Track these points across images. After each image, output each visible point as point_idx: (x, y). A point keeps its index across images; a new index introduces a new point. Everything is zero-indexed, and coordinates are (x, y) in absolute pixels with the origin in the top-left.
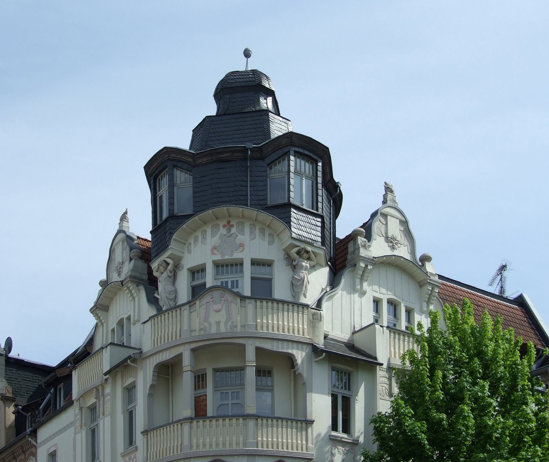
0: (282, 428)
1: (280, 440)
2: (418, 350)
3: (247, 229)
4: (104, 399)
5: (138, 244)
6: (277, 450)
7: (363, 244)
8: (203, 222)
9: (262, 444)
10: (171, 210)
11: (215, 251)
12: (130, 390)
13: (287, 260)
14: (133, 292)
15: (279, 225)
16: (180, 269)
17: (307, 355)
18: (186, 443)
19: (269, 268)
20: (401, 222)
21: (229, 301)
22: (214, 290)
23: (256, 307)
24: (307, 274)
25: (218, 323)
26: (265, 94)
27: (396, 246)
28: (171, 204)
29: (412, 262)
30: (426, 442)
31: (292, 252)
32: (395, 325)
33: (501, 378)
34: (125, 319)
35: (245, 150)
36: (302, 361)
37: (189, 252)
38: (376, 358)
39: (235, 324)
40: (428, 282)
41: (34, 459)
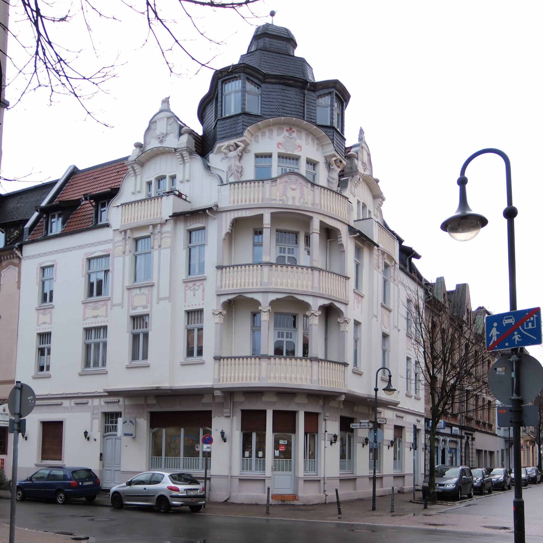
11: (280, 146)
16: (246, 151)
19: (270, 159)
37: (257, 142)
39: (306, 201)
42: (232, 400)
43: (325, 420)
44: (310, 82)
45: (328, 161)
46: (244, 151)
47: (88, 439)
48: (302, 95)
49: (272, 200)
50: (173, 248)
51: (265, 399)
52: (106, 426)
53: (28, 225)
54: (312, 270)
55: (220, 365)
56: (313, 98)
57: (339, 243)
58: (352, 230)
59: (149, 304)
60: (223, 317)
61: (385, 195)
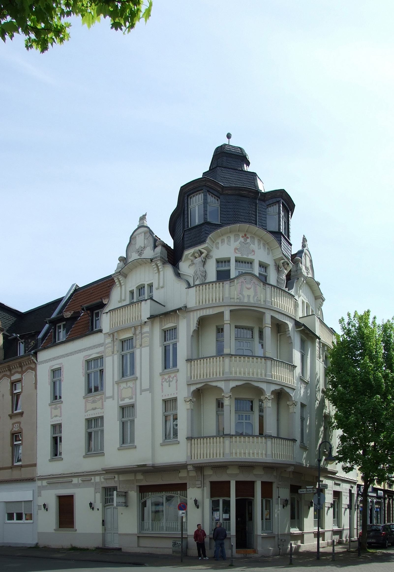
11: (237, 251)
15: (276, 243)
18: (227, 370)
21: (256, 284)
25: (249, 296)
37: (218, 248)
39: (259, 299)
42: (202, 474)
43: (278, 488)
44: (260, 193)
45: (277, 264)
46: (207, 257)
47: (93, 509)
48: (254, 204)
49: (231, 299)
50: (151, 346)
51: (229, 471)
52: (106, 498)
53: (40, 336)
54: (265, 360)
55: (191, 445)
56: (264, 207)
57: (288, 336)
58: (297, 324)
59: (134, 395)
60: (193, 404)
61: (324, 296)
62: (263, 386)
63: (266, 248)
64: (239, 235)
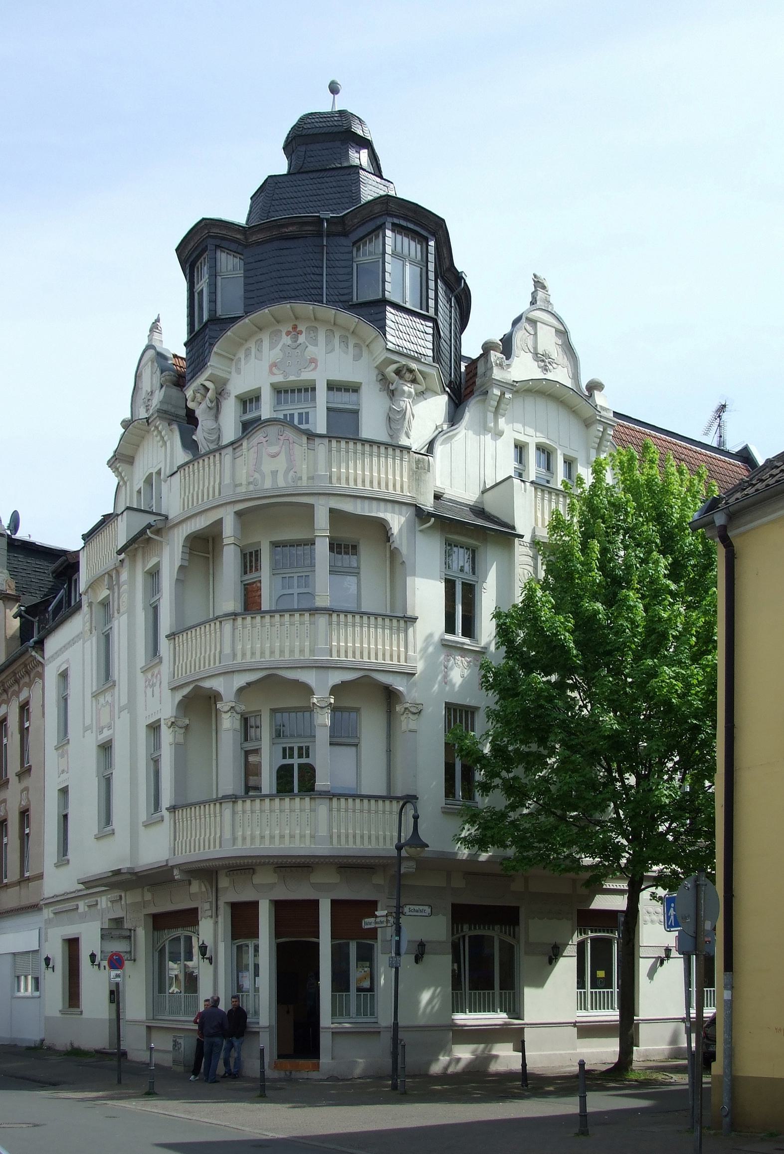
0: (369, 627)
1: (365, 645)
2: (565, 513)
3: (322, 337)
4: (119, 590)
5: (174, 365)
6: (361, 660)
7: (498, 362)
8: (258, 328)
9: (338, 652)
10: (213, 311)
11: (275, 370)
12: (154, 574)
13: (381, 382)
14: (163, 433)
15: (368, 330)
17: (407, 521)
18: (227, 650)
20: (558, 331)
21: (291, 441)
22: (269, 425)
23: (330, 451)
24: (411, 404)
25: (274, 473)
26: (357, 145)
27: (550, 367)
28: (213, 301)
29: (573, 390)
30: (572, 645)
31: (387, 370)
32: (548, 482)
33: (691, 554)
34: (154, 474)
35: (320, 220)
36: (400, 530)
37: (238, 371)
38: (513, 528)
40: (598, 420)
41: (41, 681)
51: (257, 879)
62: (309, 678)
63: (351, 346)
64: (281, 331)
